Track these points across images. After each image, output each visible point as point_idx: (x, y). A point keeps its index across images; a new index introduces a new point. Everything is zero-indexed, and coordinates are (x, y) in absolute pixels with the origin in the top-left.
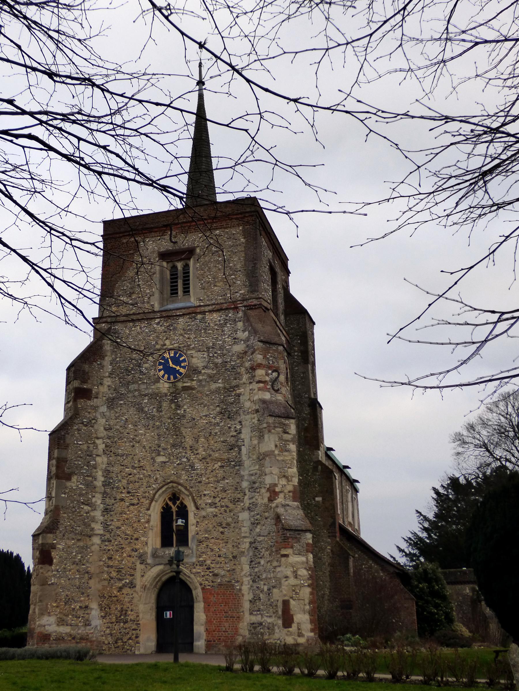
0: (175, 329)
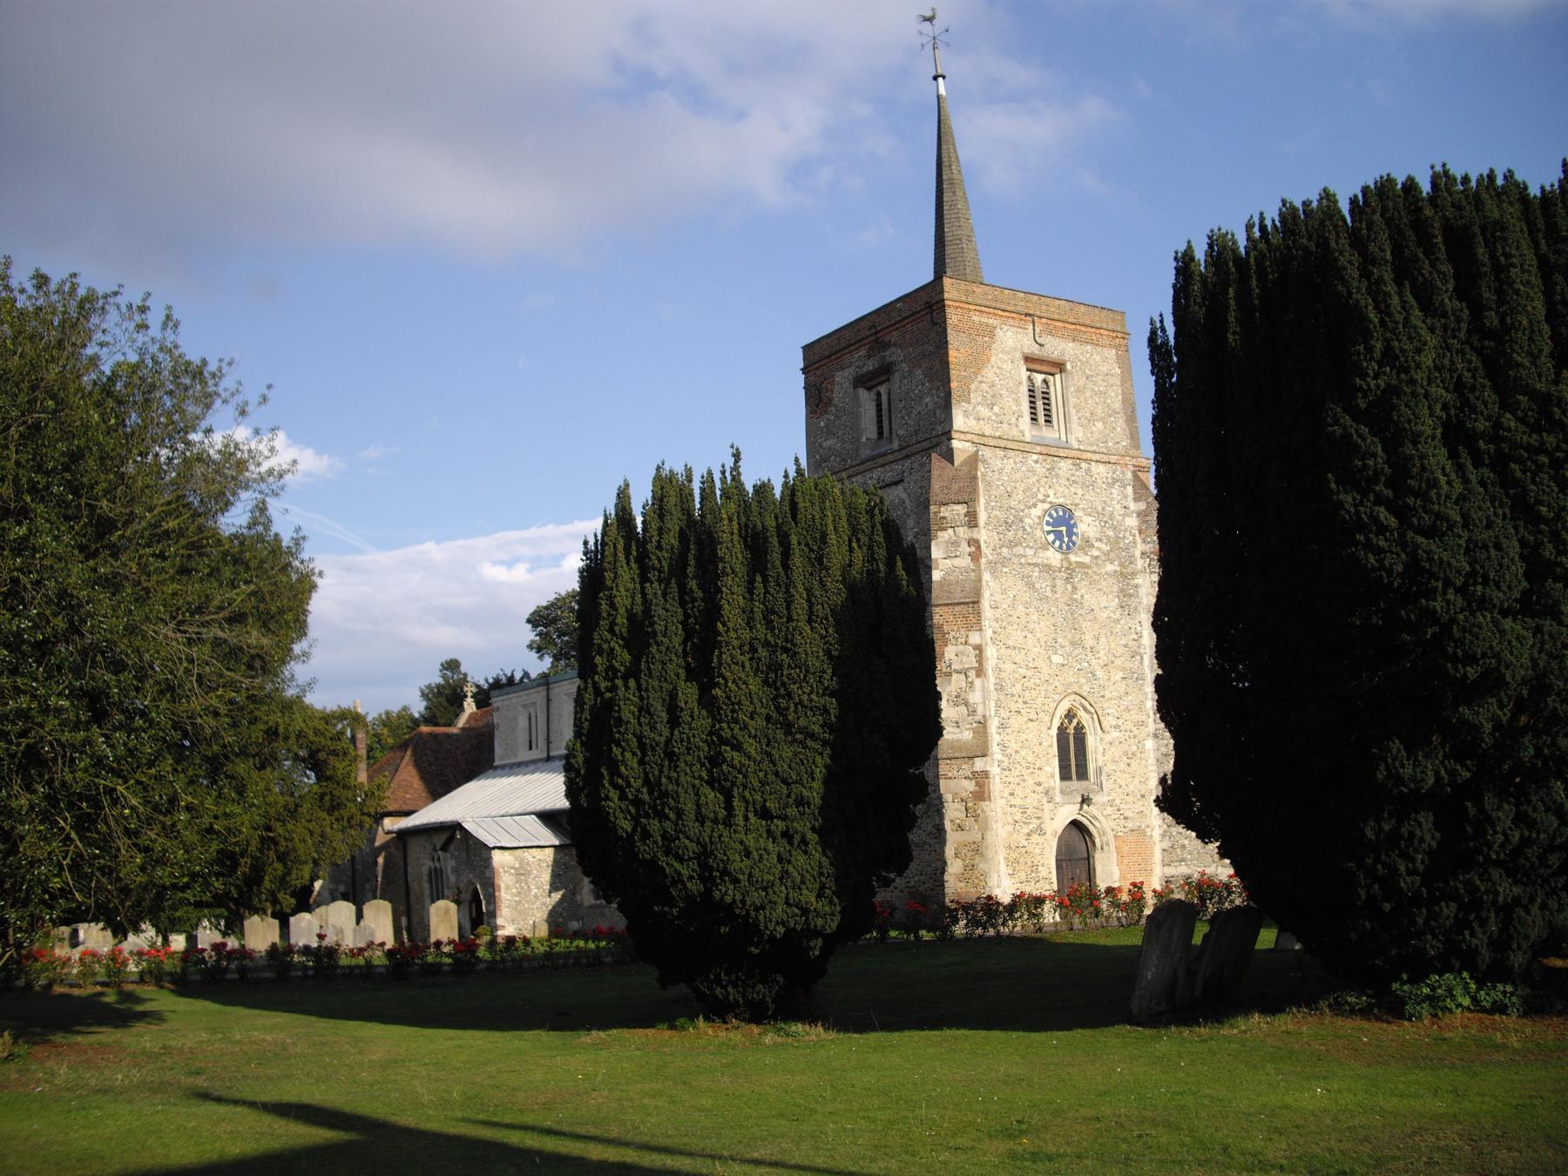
0: (1057, 475)
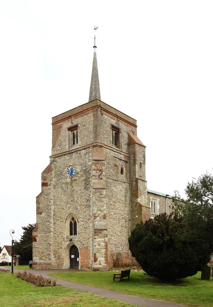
0: (72, 158)
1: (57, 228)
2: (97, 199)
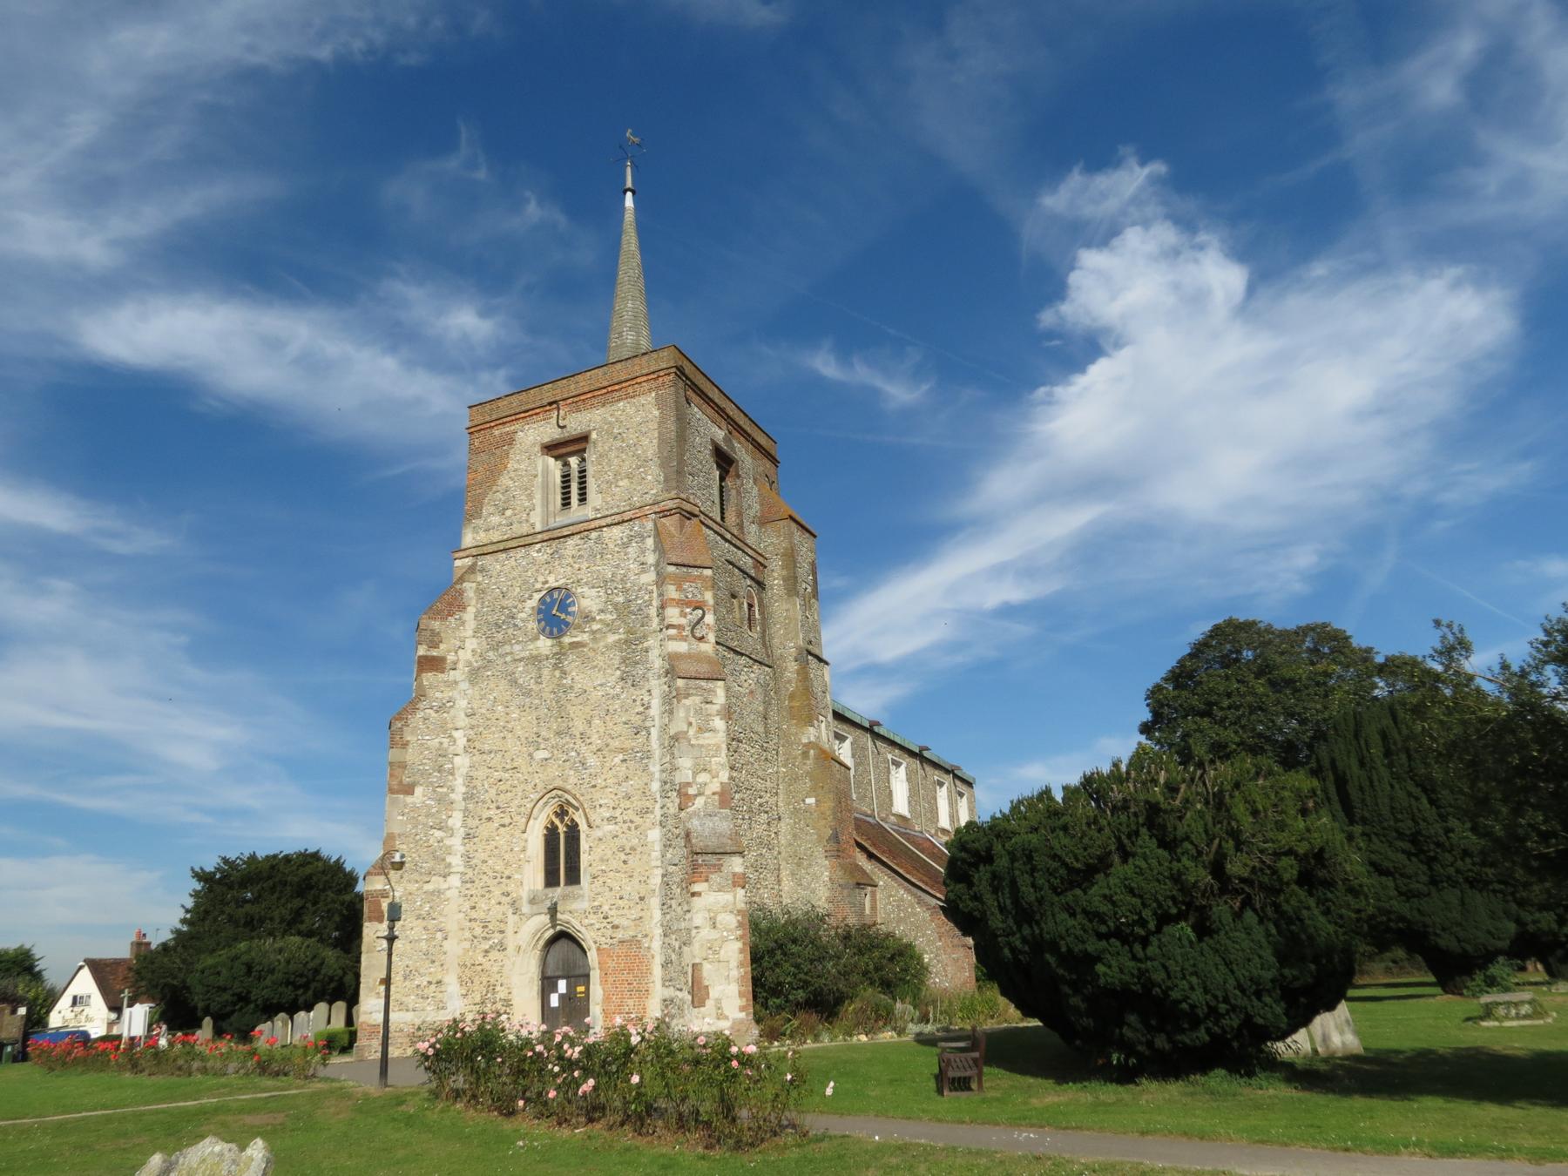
1: (483, 856)
2: (693, 720)
